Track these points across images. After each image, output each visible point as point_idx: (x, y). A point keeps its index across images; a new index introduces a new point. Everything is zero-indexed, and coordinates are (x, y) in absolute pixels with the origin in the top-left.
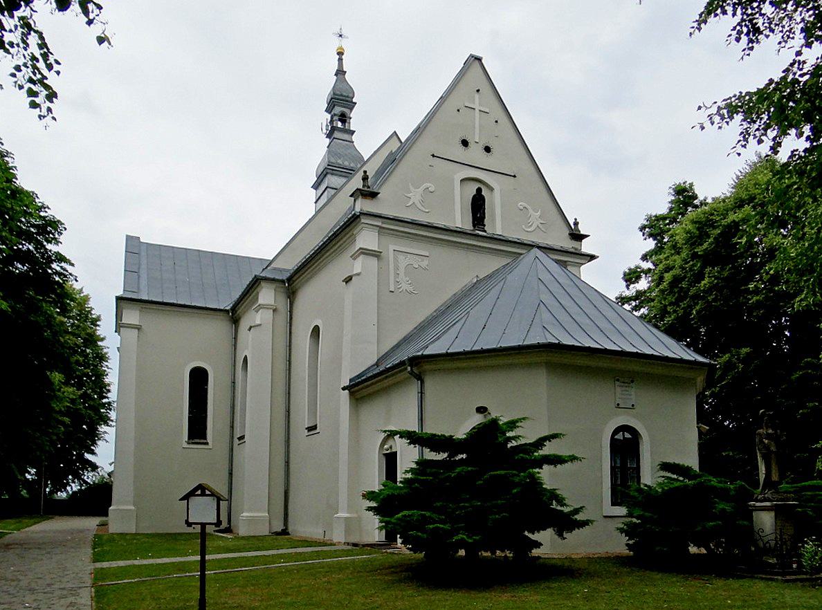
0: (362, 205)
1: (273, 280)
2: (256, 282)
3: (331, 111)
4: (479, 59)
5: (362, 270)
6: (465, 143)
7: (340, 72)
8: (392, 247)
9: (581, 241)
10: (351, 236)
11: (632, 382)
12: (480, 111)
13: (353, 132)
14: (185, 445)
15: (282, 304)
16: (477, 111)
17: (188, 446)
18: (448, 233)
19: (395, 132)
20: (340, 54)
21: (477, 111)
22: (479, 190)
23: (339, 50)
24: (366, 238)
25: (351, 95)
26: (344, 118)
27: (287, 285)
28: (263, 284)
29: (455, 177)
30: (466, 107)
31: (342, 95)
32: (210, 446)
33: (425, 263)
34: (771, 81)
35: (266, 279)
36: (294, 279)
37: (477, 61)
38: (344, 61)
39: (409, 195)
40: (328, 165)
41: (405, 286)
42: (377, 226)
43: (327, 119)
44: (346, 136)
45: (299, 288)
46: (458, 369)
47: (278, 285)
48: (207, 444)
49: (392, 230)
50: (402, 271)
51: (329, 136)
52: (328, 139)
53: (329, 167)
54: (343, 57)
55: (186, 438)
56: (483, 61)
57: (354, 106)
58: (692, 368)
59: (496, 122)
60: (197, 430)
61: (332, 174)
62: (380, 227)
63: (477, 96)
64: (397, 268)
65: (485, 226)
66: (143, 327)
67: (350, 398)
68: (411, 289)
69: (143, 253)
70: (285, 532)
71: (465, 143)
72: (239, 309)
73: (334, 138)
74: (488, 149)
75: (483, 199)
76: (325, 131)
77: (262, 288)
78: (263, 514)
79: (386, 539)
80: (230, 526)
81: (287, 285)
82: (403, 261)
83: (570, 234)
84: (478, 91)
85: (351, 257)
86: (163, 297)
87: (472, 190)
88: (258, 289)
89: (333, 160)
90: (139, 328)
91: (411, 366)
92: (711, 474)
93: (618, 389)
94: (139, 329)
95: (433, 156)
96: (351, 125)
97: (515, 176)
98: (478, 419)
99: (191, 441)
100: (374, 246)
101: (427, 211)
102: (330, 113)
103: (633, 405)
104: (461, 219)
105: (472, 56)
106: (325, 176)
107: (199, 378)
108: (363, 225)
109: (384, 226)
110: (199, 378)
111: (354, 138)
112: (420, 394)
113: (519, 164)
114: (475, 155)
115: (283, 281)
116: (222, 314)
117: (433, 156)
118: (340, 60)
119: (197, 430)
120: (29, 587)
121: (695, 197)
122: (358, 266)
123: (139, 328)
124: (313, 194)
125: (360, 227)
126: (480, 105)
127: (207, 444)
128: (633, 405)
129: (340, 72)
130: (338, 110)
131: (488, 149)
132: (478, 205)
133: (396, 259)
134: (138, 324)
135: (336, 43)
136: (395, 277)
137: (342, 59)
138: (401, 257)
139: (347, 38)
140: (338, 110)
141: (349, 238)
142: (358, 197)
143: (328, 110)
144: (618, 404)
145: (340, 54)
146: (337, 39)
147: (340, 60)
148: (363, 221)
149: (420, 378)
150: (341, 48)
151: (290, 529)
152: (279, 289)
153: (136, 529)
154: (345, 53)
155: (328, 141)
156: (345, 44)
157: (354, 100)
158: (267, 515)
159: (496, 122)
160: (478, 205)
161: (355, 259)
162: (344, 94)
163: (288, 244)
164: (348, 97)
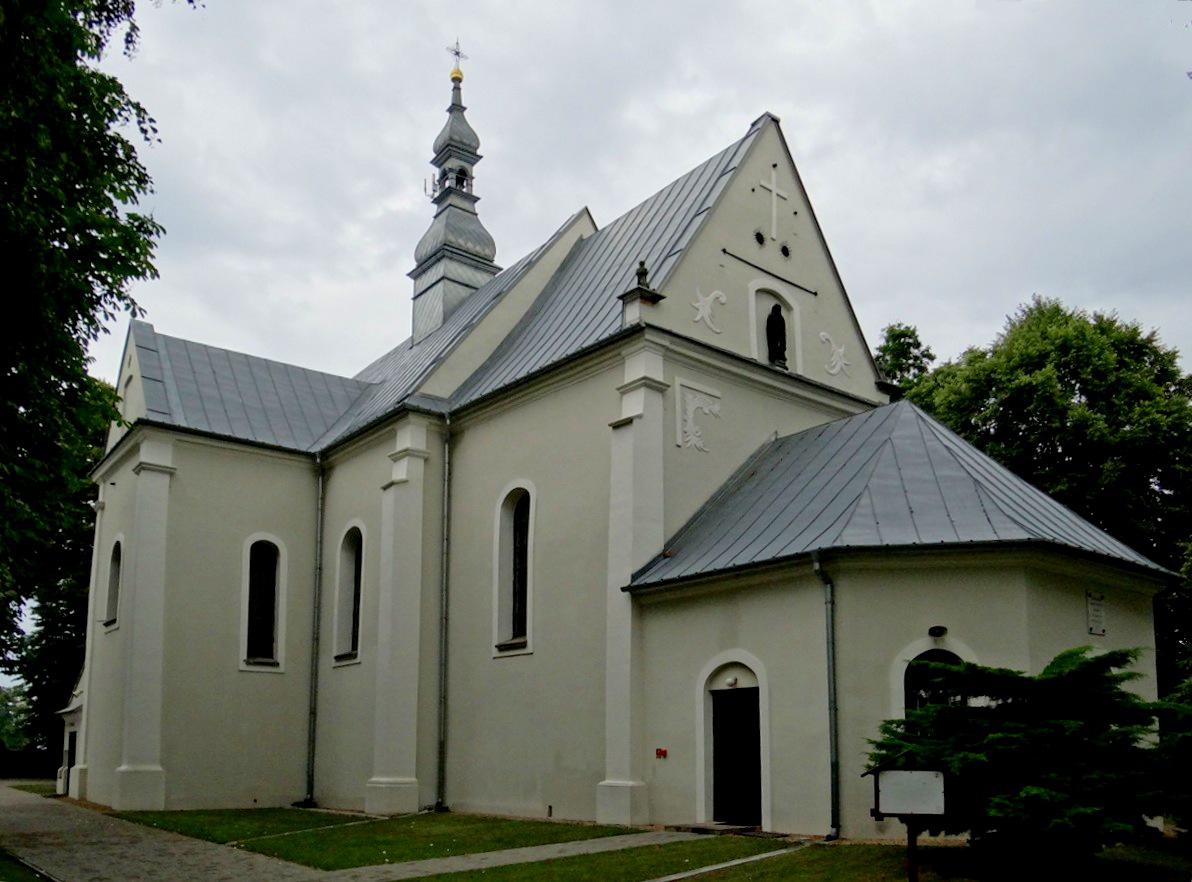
0: (635, 314)
1: (427, 413)
2: (400, 413)
3: (442, 164)
4: (776, 121)
5: (644, 410)
6: (760, 238)
7: (457, 108)
8: (678, 381)
10: (616, 356)
11: (1102, 598)
12: (778, 195)
13: (476, 199)
14: (243, 666)
15: (436, 451)
17: (338, 664)
18: (749, 367)
19: (587, 209)
20: (457, 80)
21: (774, 194)
22: (776, 310)
23: (454, 76)
24: (642, 363)
25: (474, 144)
26: (463, 176)
27: (448, 422)
28: (412, 417)
29: (749, 285)
30: (762, 186)
31: (462, 143)
32: (281, 669)
33: (716, 408)
34: (145, 169)
35: (417, 411)
36: (462, 414)
37: (773, 124)
38: (462, 91)
39: (696, 305)
41: (694, 440)
42: (663, 346)
43: (434, 175)
44: (465, 205)
45: (468, 428)
46: (891, 571)
47: (432, 421)
48: (276, 664)
49: (680, 354)
50: (690, 415)
51: (437, 201)
52: (435, 206)
53: (446, 247)
55: (244, 656)
56: (781, 124)
57: (477, 161)
59: (796, 213)
60: (261, 645)
61: (451, 258)
62: (667, 349)
63: (774, 173)
64: (685, 411)
65: (785, 360)
66: (177, 472)
67: (633, 606)
68: (700, 444)
69: (163, 352)
70: (310, 802)
71: (760, 238)
72: (332, 455)
73: (450, 205)
74: (785, 251)
76: (430, 192)
77: (409, 423)
78: (407, 780)
79: (719, 814)
80: (312, 795)
81: (448, 422)
82: (694, 402)
83: (876, 383)
84: (775, 166)
86: (209, 424)
87: (769, 304)
88: (400, 424)
89: (452, 238)
90: (170, 472)
91: (821, 562)
92: (1160, 722)
93: (1091, 608)
94: (172, 474)
95: (724, 251)
96: (474, 188)
97: (815, 294)
98: (924, 644)
99: (251, 661)
100: (659, 377)
101: (718, 331)
102: (439, 166)
103: (1104, 631)
104: (756, 348)
105: (768, 115)
106: (439, 260)
107: (264, 558)
108: (647, 343)
109: (673, 347)
110: (264, 558)
111: (478, 207)
112: (830, 606)
113: (821, 280)
114: (770, 257)
115: (441, 417)
116: (295, 462)
117: (724, 251)
118: (457, 89)
119: (261, 645)
121: (917, 345)
122: (634, 405)
123: (170, 472)
124: (409, 286)
125: (641, 345)
127: (276, 664)
128: (1104, 631)
129: (457, 108)
130: (454, 163)
131: (785, 251)
132: (776, 330)
133: (683, 395)
134: (170, 465)
135: (449, 65)
137: (459, 89)
138: (689, 396)
139: (467, 58)
140: (454, 163)
141: (597, 364)
142: (635, 299)
143: (436, 162)
144: (1091, 629)
145: (457, 80)
146: (452, 58)
147: (457, 89)
148: (647, 336)
149: (827, 579)
150: (458, 72)
151: (449, 802)
152: (433, 428)
153: (167, 798)
154: (464, 80)
155: (434, 209)
156: (465, 68)
158: (414, 779)
160: (776, 330)
162: (465, 141)
164: (469, 145)
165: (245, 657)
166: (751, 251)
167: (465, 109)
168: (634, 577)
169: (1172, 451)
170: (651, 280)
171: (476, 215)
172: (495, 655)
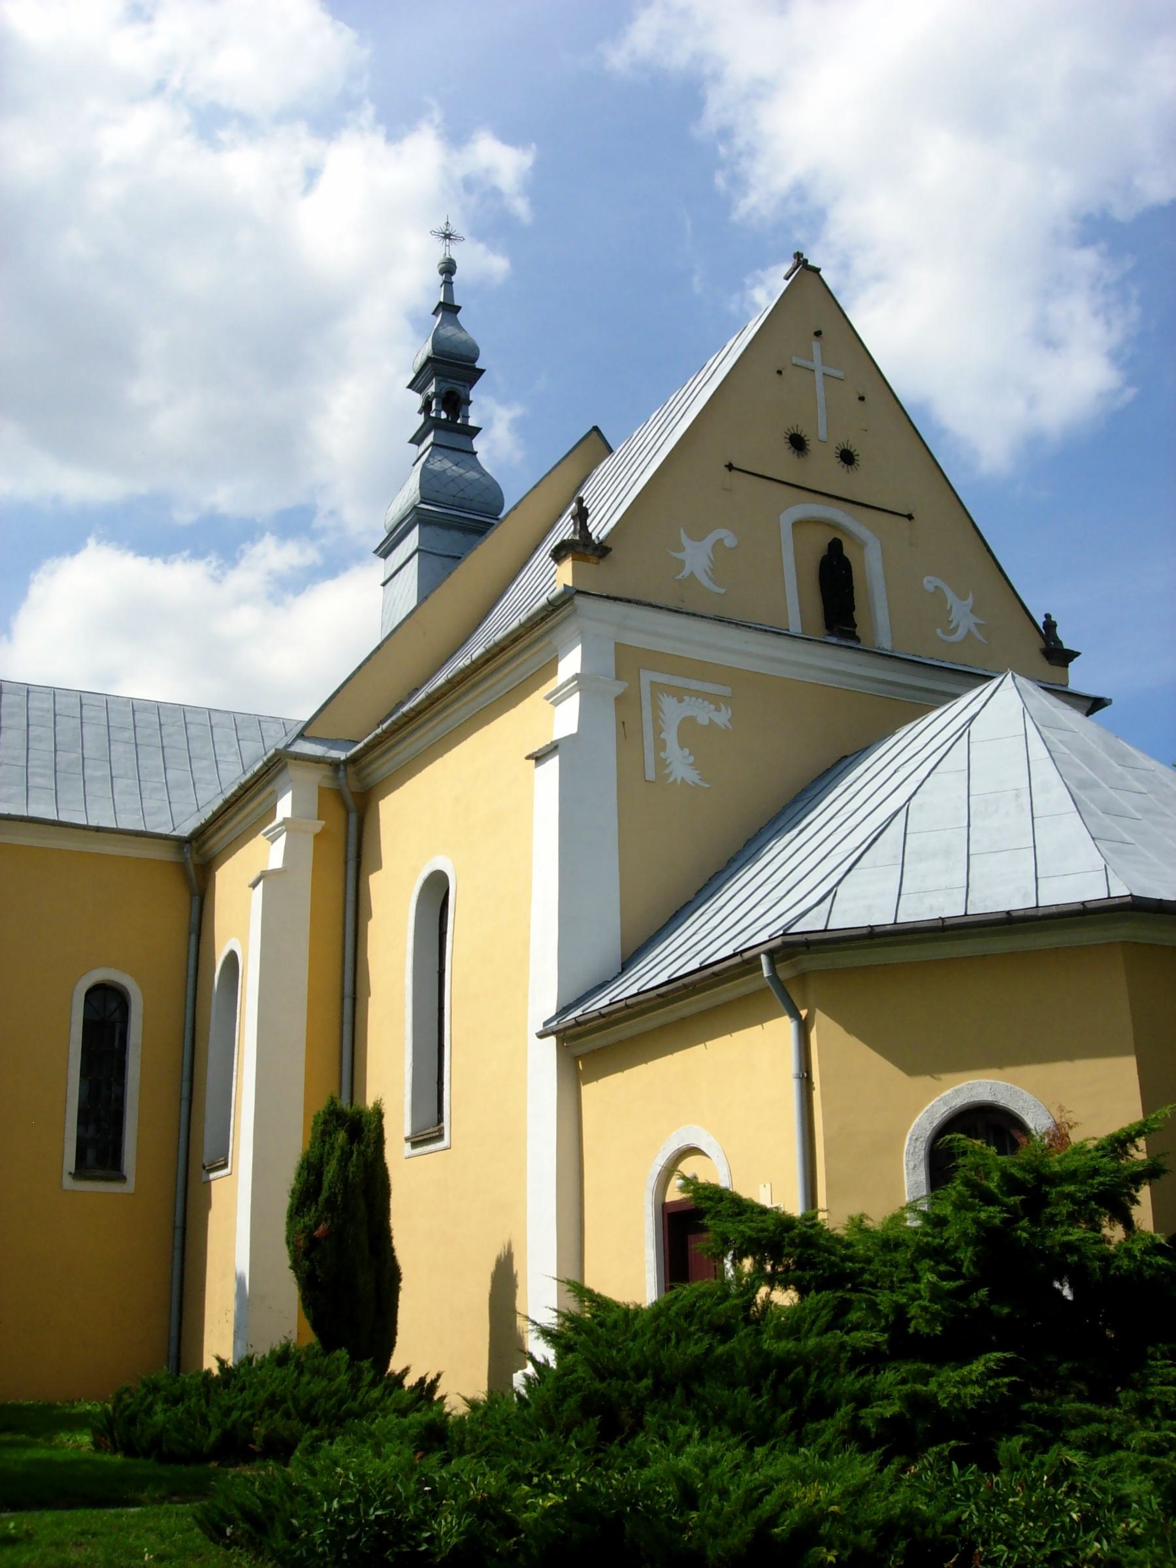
6: (798, 443)
9: (1067, 667)
16: (818, 376)
21: (818, 376)
40: (421, 502)
50: (671, 736)
54: (454, 278)
58: (174, 1228)
63: (816, 346)
71: (798, 443)
74: (847, 457)
75: (846, 565)
84: (818, 334)
85: (547, 698)
87: (818, 543)
95: (730, 467)
97: (910, 517)
102: (420, 391)
117: (730, 467)
118: (448, 284)
120: (777, 1448)
126: (824, 363)
131: (847, 457)
135: (438, 252)
136: (657, 754)
138: (668, 704)
156: (456, 252)
157: (478, 365)
159: (862, 399)
161: (556, 703)
163: (360, 667)
165: (73, 1170)
166: (784, 463)
167: (459, 308)
168: (700, 964)
169: (1100, 1190)
170: (507, 515)
171: (475, 453)
172: (406, 1155)
